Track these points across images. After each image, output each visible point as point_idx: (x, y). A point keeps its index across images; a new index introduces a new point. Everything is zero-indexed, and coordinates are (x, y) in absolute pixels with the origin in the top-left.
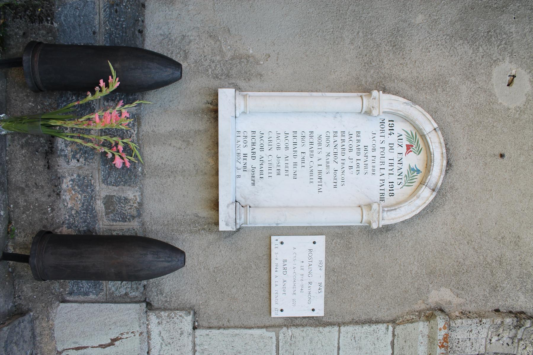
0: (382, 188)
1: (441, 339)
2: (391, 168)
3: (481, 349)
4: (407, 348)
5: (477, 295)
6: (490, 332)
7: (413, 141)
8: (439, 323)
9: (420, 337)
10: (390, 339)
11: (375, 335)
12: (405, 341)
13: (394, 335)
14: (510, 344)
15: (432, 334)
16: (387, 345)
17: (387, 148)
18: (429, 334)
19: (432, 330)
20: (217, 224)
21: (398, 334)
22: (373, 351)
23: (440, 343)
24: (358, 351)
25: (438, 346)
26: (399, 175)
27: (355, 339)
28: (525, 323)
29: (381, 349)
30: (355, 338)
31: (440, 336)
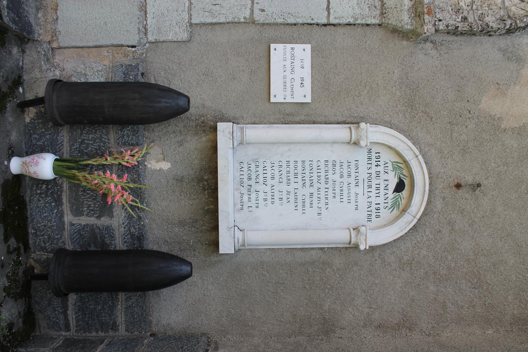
0: (369, 209)
2: (378, 191)
7: (399, 171)
17: (374, 175)
20: (216, 244)
26: (385, 200)
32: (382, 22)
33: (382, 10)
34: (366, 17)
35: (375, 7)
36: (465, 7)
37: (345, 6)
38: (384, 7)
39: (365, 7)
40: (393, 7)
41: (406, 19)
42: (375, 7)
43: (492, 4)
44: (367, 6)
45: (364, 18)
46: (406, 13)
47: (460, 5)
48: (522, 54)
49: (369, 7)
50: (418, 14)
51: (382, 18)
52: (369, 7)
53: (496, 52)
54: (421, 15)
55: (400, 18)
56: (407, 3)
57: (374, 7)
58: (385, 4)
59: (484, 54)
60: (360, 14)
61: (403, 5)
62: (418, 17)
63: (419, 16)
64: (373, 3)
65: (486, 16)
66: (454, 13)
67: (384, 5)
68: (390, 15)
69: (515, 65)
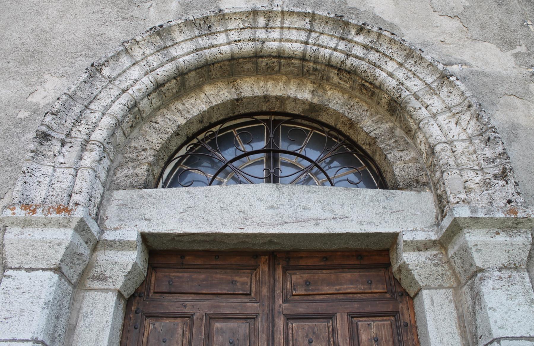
1: (25, 212)
3: (67, 173)
4: (34, 252)
5: (9, 178)
6: (48, 164)
8: (5, 216)
9: (23, 236)
10: (23, 272)
11: (11, 292)
12: (27, 254)
13: (20, 268)
14: (71, 145)
15: (20, 223)
16: (29, 277)
18: (20, 227)
19: (15, 223)
21: (18, 264)
22: (33, 294)
23: (29, 213)
24: (25, 313)
25: (33, 216)
27: (8, 318)
28: (40, 130)
29: (33, 284)
30: (5, 319)
31: (22, 213)
32: (525, 268)
33: (511, 268)
34: (525, 289)
35: (510, 277)
36: (480, 177)
37: (520, 315)
38: (508, 266)
39: (514, 291)
40: (508, 255)
41: (522, 239)
42: (510, 277)
43: (468, 151)
44: (512, 288)
45: (528, 291)
46: (515, 239)
47: (479, 182)
48: (507, 125)
49: (512, 285)
50: (515, 225)
51: (521, 268)
52: (512, 285)
53: (513, 148)
54: (517, 222)
55: (521, 246)
56: (503, 238)
57: (510, 279)
58: (504, 265)
59: (519, 159)
60: (524, 296)
61: (506, 242)
62: (518, 226)
63: (517, 224)
64: (506, 280)
65: (485, 156)
66: (493, 187)
67: (505, 267)
68: (517, 259)
69: (520, 131)
